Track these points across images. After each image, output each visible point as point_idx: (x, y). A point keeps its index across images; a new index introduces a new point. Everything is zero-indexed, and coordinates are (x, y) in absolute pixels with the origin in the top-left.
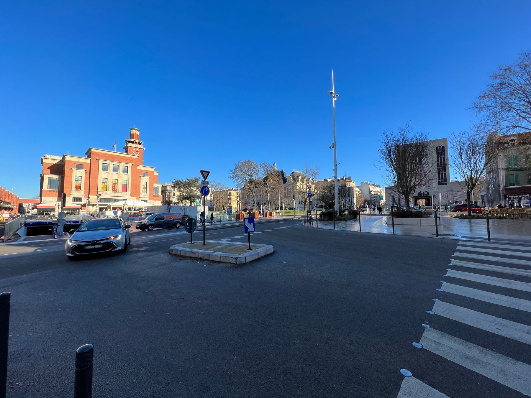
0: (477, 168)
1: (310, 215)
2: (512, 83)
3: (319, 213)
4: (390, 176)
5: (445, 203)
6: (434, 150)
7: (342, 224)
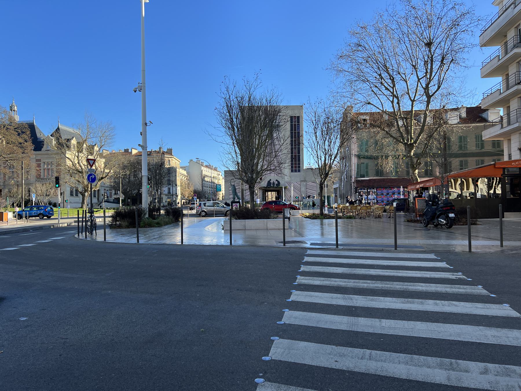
0: (331, 151)
1: (91, 216)
2: (367, 47)
3: (110, 213)
4: (230, 153)
5: (297, 198)
6: (286, 121)
7: (155, 232)
